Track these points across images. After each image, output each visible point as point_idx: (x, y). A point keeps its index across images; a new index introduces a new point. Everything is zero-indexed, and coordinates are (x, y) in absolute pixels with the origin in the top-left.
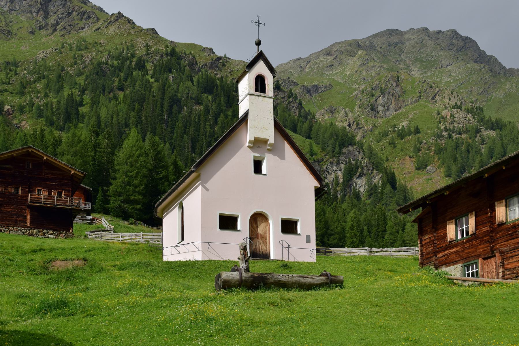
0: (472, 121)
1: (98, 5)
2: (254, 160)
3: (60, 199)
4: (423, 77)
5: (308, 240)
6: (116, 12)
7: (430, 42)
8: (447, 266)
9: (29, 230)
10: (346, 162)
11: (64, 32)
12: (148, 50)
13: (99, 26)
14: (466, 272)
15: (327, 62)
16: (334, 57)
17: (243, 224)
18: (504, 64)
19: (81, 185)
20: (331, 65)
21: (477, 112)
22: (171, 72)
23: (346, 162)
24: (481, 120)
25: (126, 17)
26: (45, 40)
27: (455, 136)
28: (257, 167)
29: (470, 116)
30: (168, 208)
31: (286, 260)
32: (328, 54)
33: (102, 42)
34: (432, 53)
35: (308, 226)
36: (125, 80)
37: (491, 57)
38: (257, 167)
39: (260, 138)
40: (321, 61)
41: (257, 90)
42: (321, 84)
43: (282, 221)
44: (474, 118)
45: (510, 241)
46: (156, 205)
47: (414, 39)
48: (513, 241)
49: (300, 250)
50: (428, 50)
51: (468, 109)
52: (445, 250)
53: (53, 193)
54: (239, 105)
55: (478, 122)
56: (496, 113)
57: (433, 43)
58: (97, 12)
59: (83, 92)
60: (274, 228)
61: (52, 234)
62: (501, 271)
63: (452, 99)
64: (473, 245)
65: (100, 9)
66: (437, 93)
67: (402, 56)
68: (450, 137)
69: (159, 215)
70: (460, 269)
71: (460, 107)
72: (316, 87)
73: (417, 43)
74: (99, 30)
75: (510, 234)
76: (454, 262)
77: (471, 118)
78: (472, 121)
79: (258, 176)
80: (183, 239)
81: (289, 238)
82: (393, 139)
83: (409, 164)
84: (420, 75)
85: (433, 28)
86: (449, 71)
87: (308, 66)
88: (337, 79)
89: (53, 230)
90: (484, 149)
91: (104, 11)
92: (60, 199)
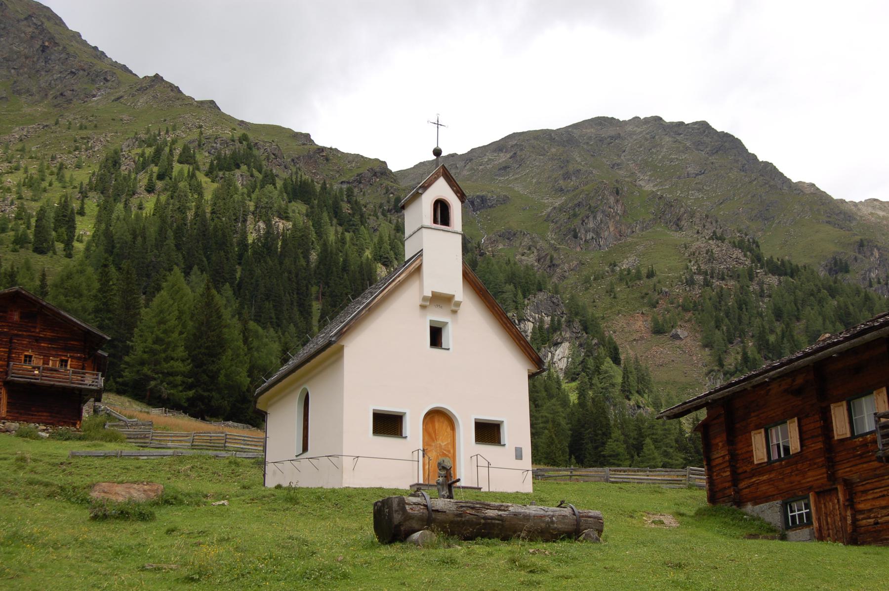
0: (742, 261)
1: (121, 61)
2: (431, 327)
3: (68, 373)
4: (658, 191)
5: (519, 455)
6: (152, 74)
7: (667, 139)
8: (756, 504)
9: (4, 423)
10: (534, 318)
11: (60, 100)
12: (201, 133)
13: (121, 94)
14: (790, 514)
15: (501, 161)
16: (511, 154)
17: (413, 426)
18: (787, 174)
19: (100, 352)
20: (505, 168)
21: (750, 247)
22: (238, 167)
23: (534, 318)
24: (758, 259)
25: (167, 82)
26: (26, 110)
27: (716, 283)
28: (436, 336)
29: (737, 253)
30: (282, 395)
31: (485, 489)
32: (501, 150)
33: (125, 117)
34: (671, 154)
35: (518, 431)
36: (161, 177)
37: (767, 164)
38: (436, 336)
39: (441, 294)
40: (489, 160)
41: (435, 222)
42: (490, 195)
43: (476, 423)
44: (745, 256)
45: (860, 466)
46: (258, 390)
47: (641, 132)
48: (865, 465)
49: (504, 473)
50: (665, 150)
51: (734, 243)
52: (751, 477)
53: (51, 362)
54: (406, 243)
55: (753, 262)
56: (781, 249)
57: (671, 139)
58: (119, 72)
59: (84, 195)
60: (466, 433)
61: (44, 430)
62: (849, 513)
63: (708, 225)
64: (797, 470)
65: (124, 68)
66: (683, 215)
67: (622, 158)
68: (707, 284)
69: (259, 406)
70: (778, 509)
71: (722, 239)
72: (483, 199)
73: (646, 140)
74: (122, 100)
75: (860, 455)
76: (766, 498)
77: (741, 256)
78: (742, 261)
79: (436, 351)
80: (305, 448)
81: (488, 451)
82: (612, 284)
83: (641, 325)
84: (654, 186)
85: (668, 119)
86: (699, 183)
87: (468, 167)
88: (516, 189)
89: (46, 424)
90: (764, 306)
91: (131, 72)
92: (68, 373)
